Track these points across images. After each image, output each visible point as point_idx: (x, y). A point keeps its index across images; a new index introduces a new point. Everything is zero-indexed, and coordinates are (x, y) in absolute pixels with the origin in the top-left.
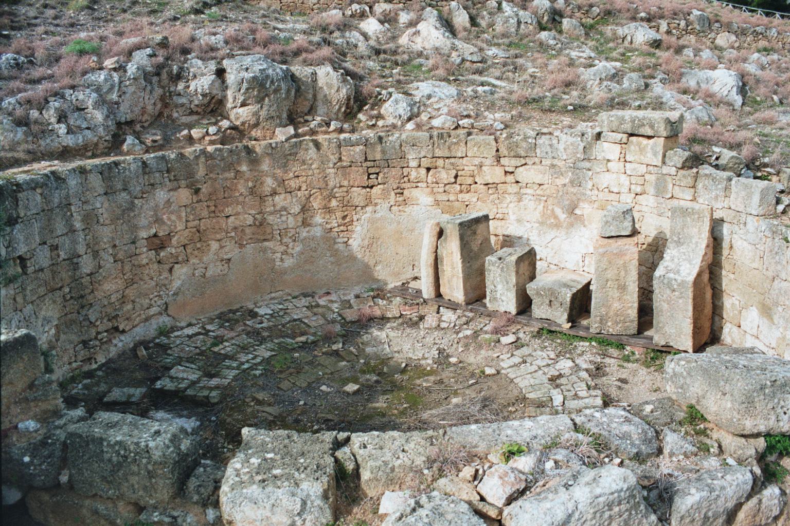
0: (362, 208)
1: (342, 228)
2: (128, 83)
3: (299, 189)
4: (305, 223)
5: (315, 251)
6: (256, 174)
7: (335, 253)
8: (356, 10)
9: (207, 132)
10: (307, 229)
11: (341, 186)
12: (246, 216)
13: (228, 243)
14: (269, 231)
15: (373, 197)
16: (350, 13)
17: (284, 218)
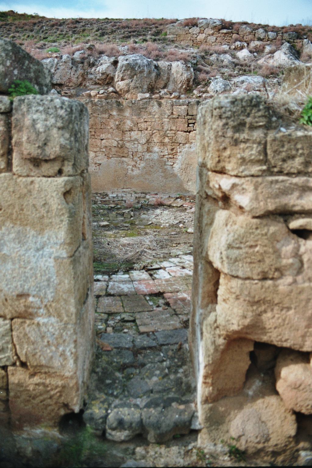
0: (184, 144)
1: (170, 156)
2: (61, 64)
3: (147, 130)
4: (148, 150)
5: (152, 168)
6: (121, 117)
7: (165, 171)
8: (238, 46)
9: (98, 92)
10: (149, 154)
11: (171, 130)
12: (113, 141)
13: (100, 155)
14: (126, 151)
15: (190, 138)
16: (233, 47)
17: (136, 146)
